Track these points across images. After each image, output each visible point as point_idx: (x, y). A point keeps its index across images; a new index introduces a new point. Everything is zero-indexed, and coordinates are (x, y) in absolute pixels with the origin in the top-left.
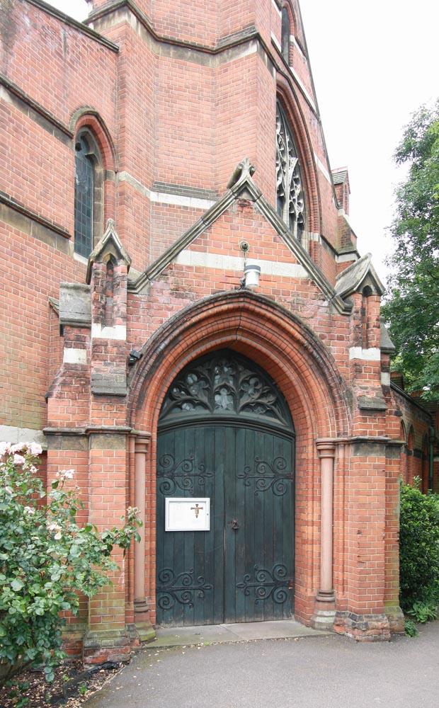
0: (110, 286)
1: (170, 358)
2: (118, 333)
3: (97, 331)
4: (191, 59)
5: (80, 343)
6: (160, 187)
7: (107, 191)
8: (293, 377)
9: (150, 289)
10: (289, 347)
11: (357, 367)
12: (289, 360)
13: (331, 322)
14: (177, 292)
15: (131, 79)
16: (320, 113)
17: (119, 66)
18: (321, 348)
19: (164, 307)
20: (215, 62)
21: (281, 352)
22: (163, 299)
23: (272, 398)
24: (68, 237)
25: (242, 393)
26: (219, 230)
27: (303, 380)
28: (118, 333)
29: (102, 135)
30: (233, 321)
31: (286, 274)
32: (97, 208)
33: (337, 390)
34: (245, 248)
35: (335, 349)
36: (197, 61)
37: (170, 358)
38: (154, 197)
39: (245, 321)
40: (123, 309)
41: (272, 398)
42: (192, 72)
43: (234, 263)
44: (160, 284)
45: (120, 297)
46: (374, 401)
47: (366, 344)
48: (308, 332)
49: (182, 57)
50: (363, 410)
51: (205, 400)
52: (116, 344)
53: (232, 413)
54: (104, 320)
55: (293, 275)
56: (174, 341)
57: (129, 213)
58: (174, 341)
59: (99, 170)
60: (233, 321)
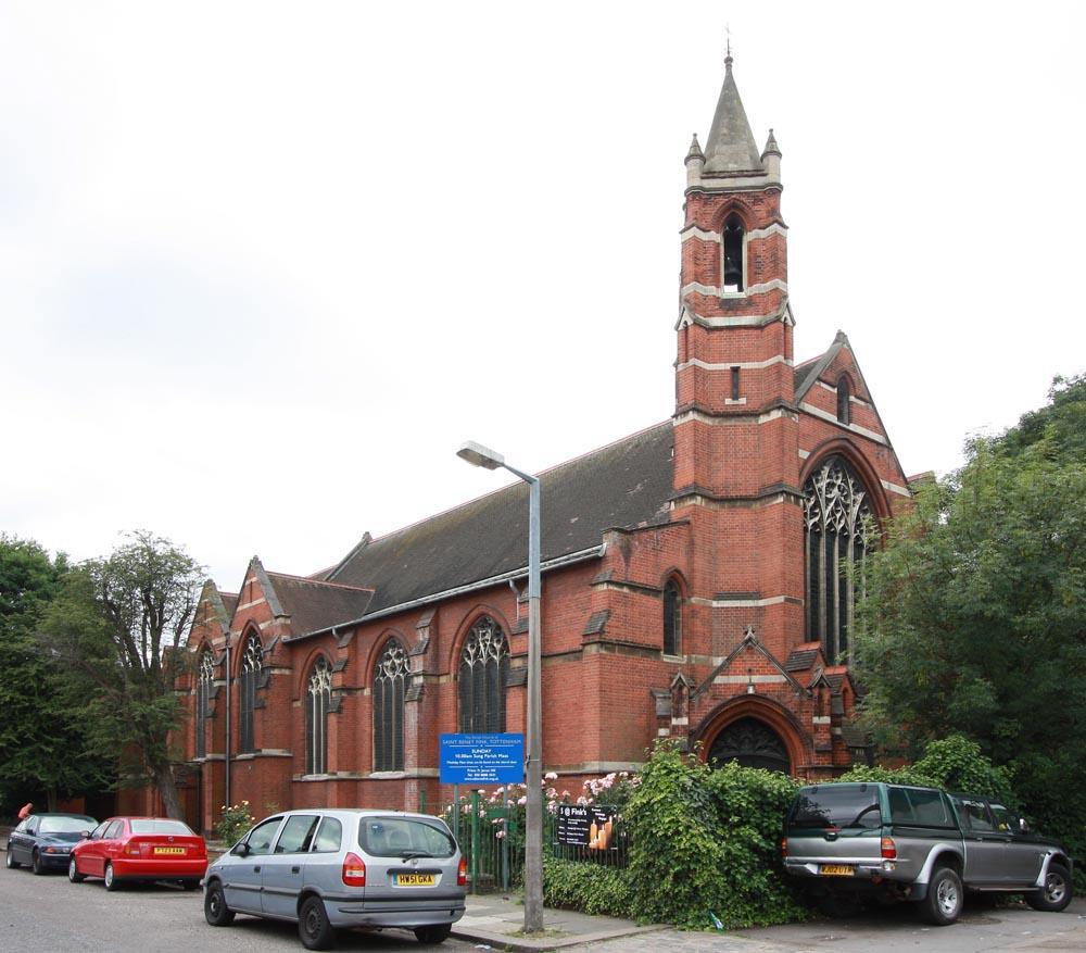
0: (680, 698)
1: (712, 729)
2: (684, 721)
3: (674, 722)
4: (740, 506)
5: (666, 726)
6: (719, 597)
7: (683, 611)
8: (782, 733)
9: (701, 698)
10: (778, 719)
11: (816, 727)
12: (779, 725)
13: (801, 703)
14: (714, 698)
15: (698, 540)
16: (892, 442)
17: (690, 531)
18: (794, 718)
19: (709, 705)
20: (757, 506)
21: (774, 721)
22: (706, 702)
23: (776, 742)
24: (658, 651)
25: (757, 741)
26: (737, 663)
27: (788, 735)
28: (684, 721)
29: (681, 579)
30: (746, 708)
31: (773, 681)
32: (678, 622)
33: (806, 739)
34: (750, 670)
35: (803, 719)
36: (744, 507)
37: (712, 729)
38: (715, 604)
39: (753, 707)
40: (687, 710)
41: (776, 742)
42: (743, 516)
43: (745, 679)
44: (704, 695)
45: (685, 705)
46: (825, 746)
47: (820, 714)
48: (786, 710)
49: (734, 507)
50: (817, 752)
51: (735, 745)
52: (683, 726)
53: (751, 752)
54: (678, 715)
55: (778, 681)
56: (714, 721)
57: (698, 622)
58: (714, 721)
59: (679, 598)
60: (746, 708)
